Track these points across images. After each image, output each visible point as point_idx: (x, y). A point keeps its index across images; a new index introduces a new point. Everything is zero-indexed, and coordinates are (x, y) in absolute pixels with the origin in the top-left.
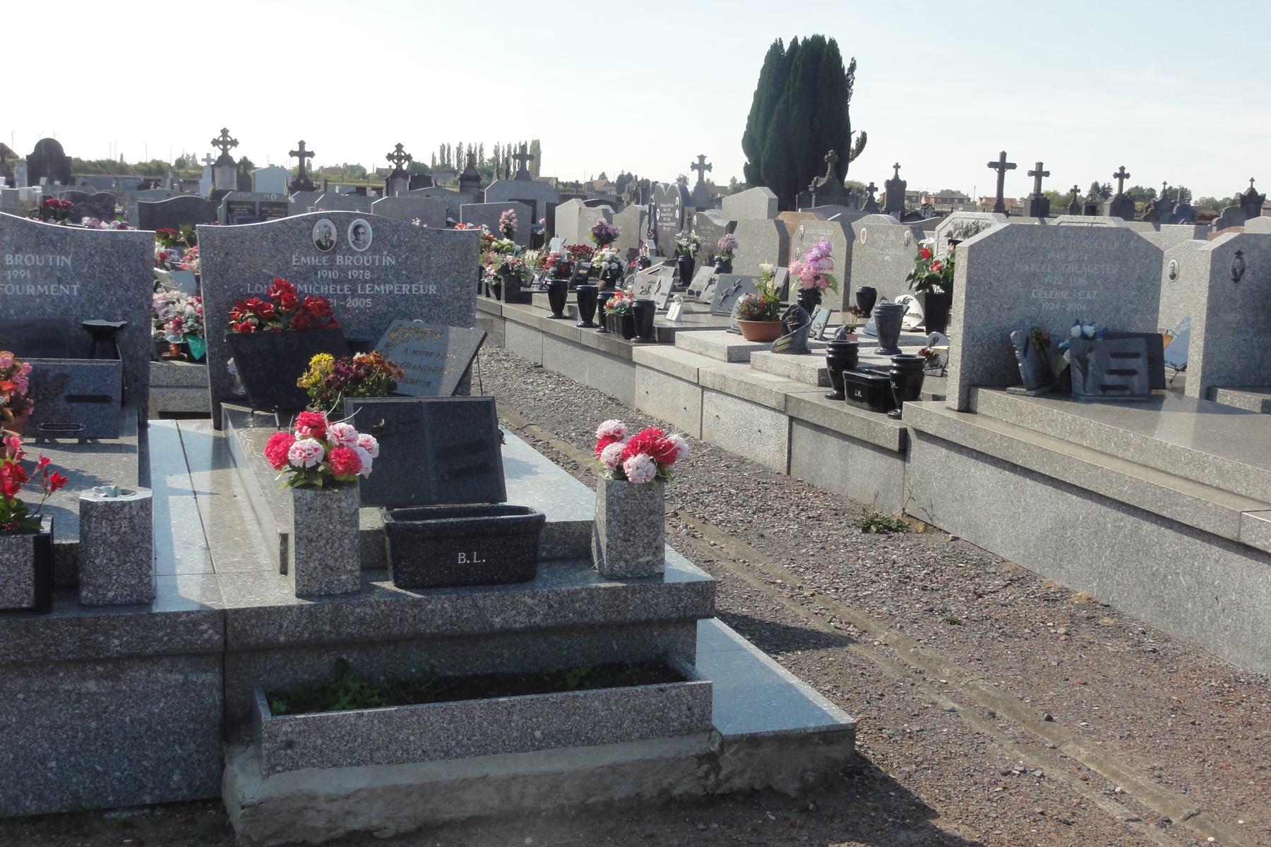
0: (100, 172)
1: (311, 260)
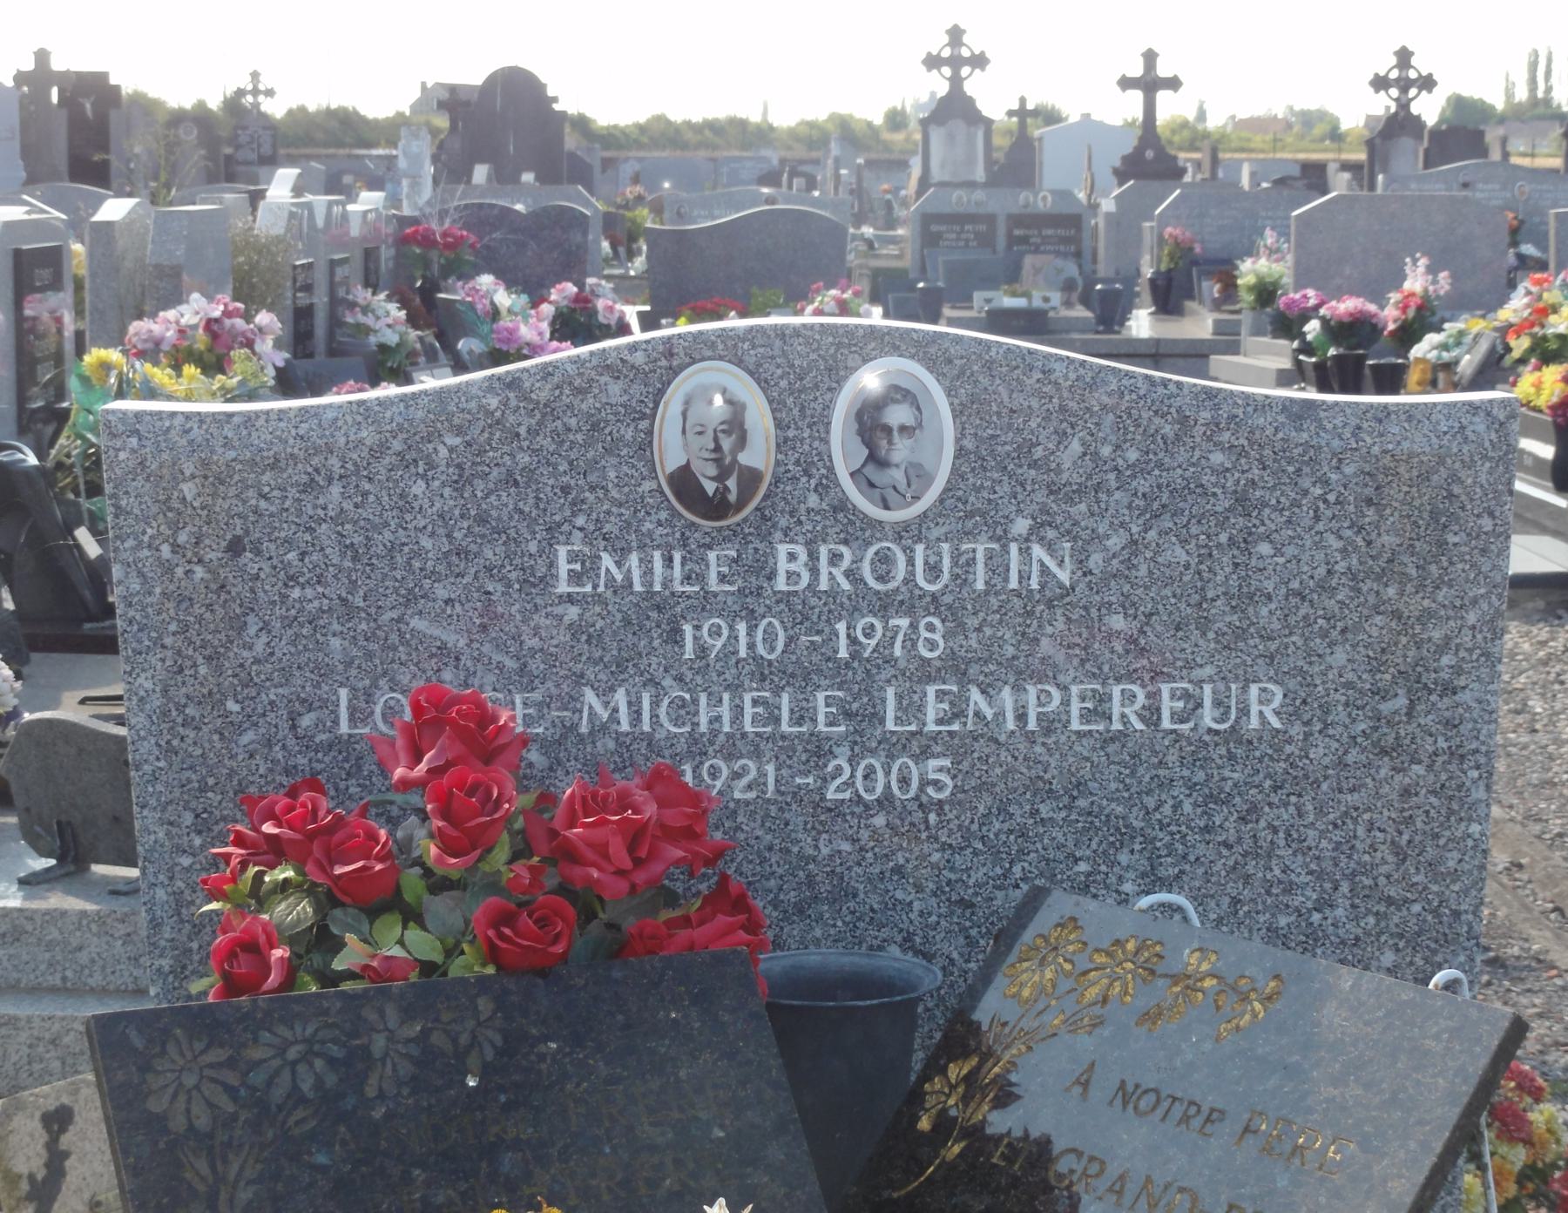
0: (715, 147)
1: (649, 571)
